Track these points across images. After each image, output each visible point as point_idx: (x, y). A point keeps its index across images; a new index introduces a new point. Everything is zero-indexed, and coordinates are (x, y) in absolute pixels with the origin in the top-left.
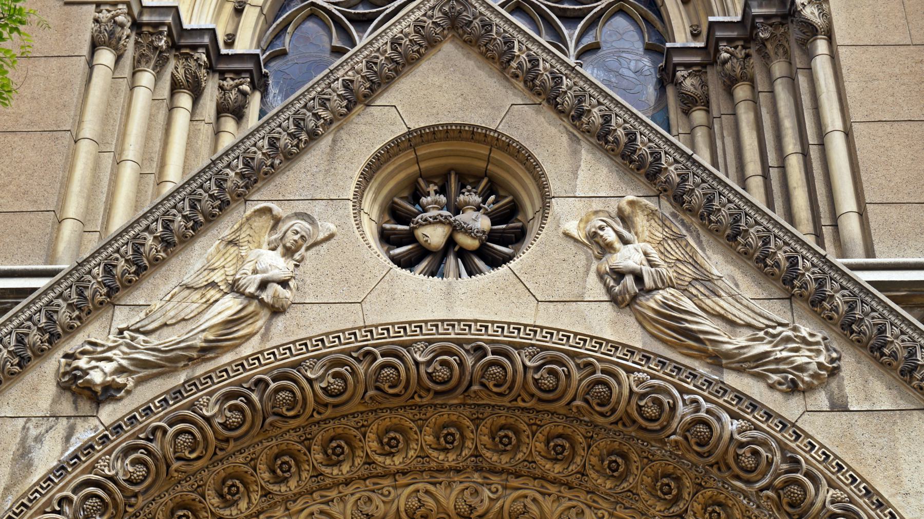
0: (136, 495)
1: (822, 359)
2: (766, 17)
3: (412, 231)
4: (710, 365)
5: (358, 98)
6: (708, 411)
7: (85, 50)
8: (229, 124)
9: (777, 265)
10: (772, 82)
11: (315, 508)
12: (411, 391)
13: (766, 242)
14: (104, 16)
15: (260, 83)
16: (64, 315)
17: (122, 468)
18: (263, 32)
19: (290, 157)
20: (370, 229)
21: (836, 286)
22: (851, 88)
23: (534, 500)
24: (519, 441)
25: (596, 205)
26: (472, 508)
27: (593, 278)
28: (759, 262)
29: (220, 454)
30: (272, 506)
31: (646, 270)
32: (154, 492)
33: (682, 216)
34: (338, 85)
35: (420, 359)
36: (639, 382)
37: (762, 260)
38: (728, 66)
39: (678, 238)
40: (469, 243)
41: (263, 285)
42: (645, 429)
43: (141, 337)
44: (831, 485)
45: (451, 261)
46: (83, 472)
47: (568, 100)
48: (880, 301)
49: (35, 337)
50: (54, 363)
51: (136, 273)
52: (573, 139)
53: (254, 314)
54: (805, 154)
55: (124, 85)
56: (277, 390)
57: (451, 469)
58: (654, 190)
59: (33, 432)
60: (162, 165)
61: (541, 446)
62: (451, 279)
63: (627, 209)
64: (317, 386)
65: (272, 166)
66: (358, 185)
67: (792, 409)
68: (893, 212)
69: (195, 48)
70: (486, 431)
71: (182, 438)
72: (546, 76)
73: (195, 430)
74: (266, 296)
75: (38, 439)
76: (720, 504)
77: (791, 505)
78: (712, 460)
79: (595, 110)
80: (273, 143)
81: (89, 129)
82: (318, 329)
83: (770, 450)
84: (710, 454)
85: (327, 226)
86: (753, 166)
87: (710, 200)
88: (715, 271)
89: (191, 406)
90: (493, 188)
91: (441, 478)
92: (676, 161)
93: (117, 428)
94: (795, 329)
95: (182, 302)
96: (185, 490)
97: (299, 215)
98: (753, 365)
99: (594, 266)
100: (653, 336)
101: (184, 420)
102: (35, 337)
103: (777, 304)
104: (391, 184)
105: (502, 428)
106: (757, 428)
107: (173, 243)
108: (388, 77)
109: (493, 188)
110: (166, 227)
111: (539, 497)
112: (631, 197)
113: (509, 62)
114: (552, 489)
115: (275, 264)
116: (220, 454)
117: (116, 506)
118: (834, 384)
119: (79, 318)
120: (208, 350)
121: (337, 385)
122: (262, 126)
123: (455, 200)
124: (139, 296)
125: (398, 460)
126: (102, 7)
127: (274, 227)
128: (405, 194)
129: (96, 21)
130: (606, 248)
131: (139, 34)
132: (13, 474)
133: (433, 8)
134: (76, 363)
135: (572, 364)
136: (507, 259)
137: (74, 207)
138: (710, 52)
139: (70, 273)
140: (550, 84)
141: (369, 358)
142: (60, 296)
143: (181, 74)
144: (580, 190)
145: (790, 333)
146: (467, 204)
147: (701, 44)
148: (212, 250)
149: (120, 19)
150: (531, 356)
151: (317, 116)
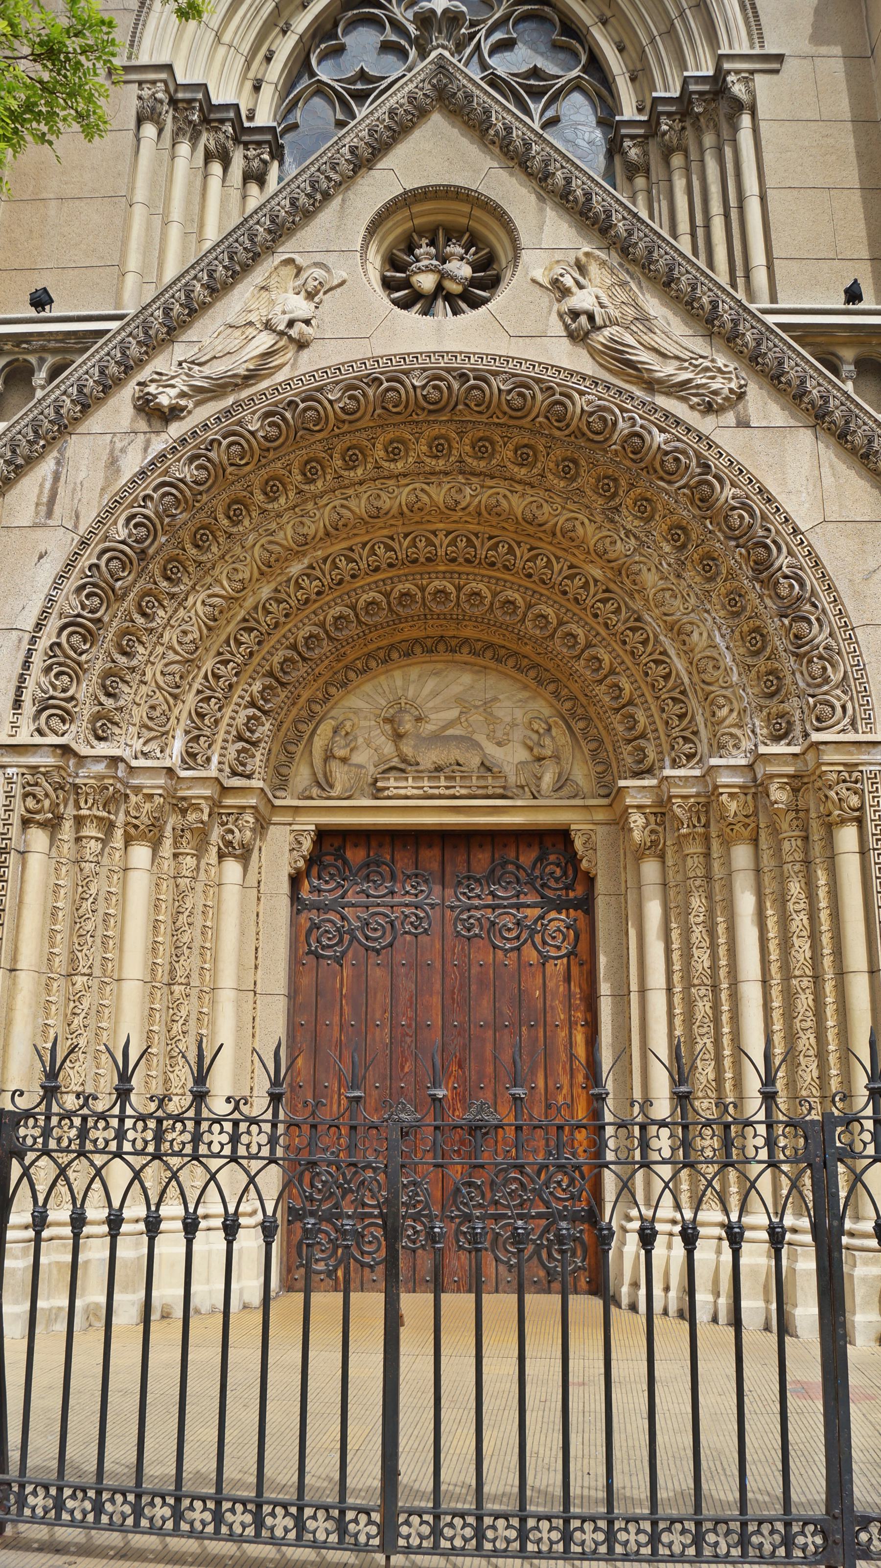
0: (201, 493)
1: (733, 385)
2: (701, 93)
3: (408, 277)
4: (645, 389)
5: (363, 161)
6: (642, 427)
7: (132, 124)
8: (253, 188)
9: (702, 307)
10: (702, 152)
11: (337, 503)
12: (410, 410)
13: (694, 289)
14: (146, 93)
15: (278, 153)
16: (134, 350)
17: (188, 472)
18: (278, 107)
19: (308, 215)
20: (375, 277)
21: (748, 325)
22: (767, 157)
23: (505, 496)
24: (493, 449)
25: (559, 255)
26: (457, 503)
27: (554, 317)
28: (688, 306)
29: (263, 461)
30: (305, 501)
31: (597, 311)
32: (214, 491)
33: (627, 266)
34: (345, 150)
35: (417, 384)
36: (589, 403)
37: (690, 304)
38: (667, 137)
39: (623, 284)
40: (455, 288)
41: (291, 324)
42: (592, 441)
43: (196, 368)
44: (733, 485)
45: (440, 302)
46: (159, 476)
47: (537, 163)
48: (782, 339)
49: (113, 369)
50: (128, 392)
51: (189, 315)
52: (541, 199)
53: (285, 348)
54: (727, 216)
55: (166, 155)
56: (305, 410)
57: (440, 472)
58: (605, 244)
59: (119, 445)
60: (202, 226)
61: (510, 454)
62: (440, 317)
63: (584, 260)
64: (336, 406)
65: (293, 222)
66: (364, 238)
67: (706, 424)
68: (794, 266)
69: (222, 121)
70: (468, 441)
71: (233, 448)
72: (519, 143)
73: (243, 442)
74: (294, 332)
75: (123, 450)
76: (647, 500)
77: (702, 500)
78: (643, 465)
79: (559, 173)
80: (293, 202)
81: (141, 194)
83: (688, 458)
84: (642, 460)
85: (340, 274)
86: (683, 226)
87: (650, 252)
88: (652, 312)
89: (239, 423)
90: (473, 241)
91: (433, 479)
92: (624, 218)
93: (183, 441)
94: (713, 361)
95: (227, 338)
96: (237, 490)
97: (317, 264)
98: (679, 390)
99: (556, 306)
100: (601, 365)
101: (234, 434)
102: (113, 369)
103: (700, 340)
104: (390, 238)
105: (480, 439)
106: (679, 440)
107: (217, 290)
108: (386, 144)
109: (473, 241)
110: (210, 276)
111: (508, 494)
112: (587, 249)
113: (487, 129)
114: (519, 488)
115: (301, 307)
116: (263, 461)
117: (186, 502)
119: (146, 353)
120: (250, 378)
121: (352, 405)
122: (280, 191)
123: (444, 249)
124: (192, 334)
125: (400, 465)
126: (144, 86)
127: (297, 275)
128: (402, 247)
129: (140, 98)
130: (565, 292)
131: (175, 110)
132: (106, 478)
133: (423, 81)
134: (147, 390)
135: (536, 388)
136: (485, 301)
137: (133, 262)
138: (652, 126)
139: (136, 316)
140: (522, 149)
141: (376, 383)
142: (130, 335)
143: (212, 146)
144: (546, 241)
145: (709, 364)
146: (452, 254)
147: (645, 118)
148: (248, 295)
149: (160, 95)
150: (505, 381)
151: (329, 179)
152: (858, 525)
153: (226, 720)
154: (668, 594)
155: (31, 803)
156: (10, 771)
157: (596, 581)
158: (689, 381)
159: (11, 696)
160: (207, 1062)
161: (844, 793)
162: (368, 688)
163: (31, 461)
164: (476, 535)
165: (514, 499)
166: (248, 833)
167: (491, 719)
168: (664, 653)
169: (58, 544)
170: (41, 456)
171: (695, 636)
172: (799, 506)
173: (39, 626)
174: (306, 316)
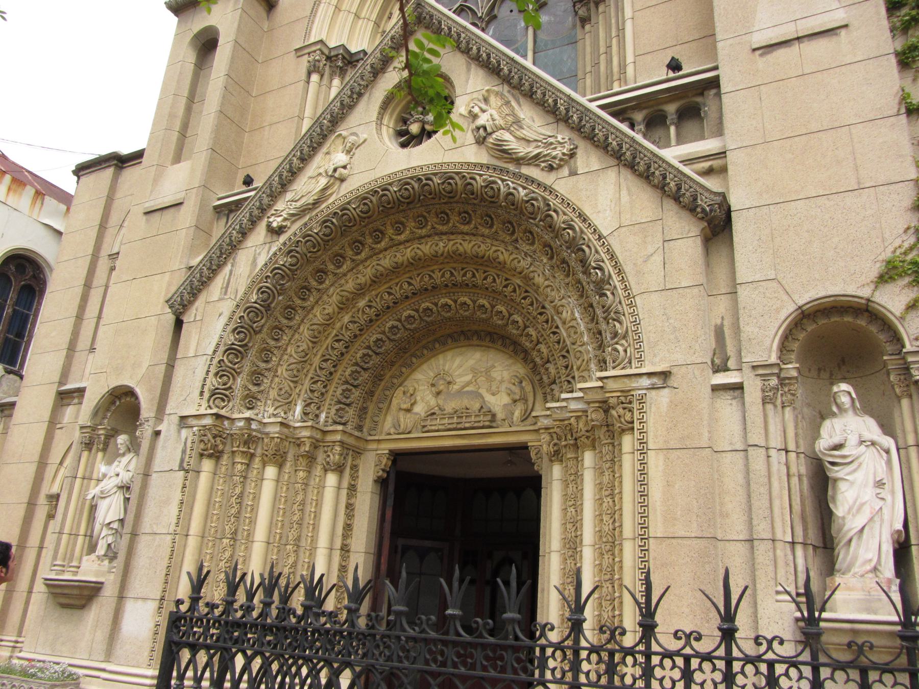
16: (266, 200)
19: (351, 107)
30: (358, 265)
36: (484, 180)
39: (508, 103)
41: (335, 170)
53: (333, 184)
74: (337, 175)
75: (259, 254)
82: (355, 186)
91: (423, 241)
95: (306, 187)
98: (534, 160)
107: (305, 159)
112: (487, 88)
114: (467, 237)
118: (572, 161)
120: (316, 203)
131: (331, 62)
152: (643, 226)
153: (331, 392)
154: (549, 289)
155: (202, 446)
156: (195, 429)
157: (519, 286)
158: (539, 154)
159: (199, 390)
160: (290, 589)
161: (621, 411)
162: (425, 367)
163: (220, 266)
164: (454, 269)
165: (465, 244)
166: (337, 457)
167: (490, 379)
168: (557, 327)
169: (227, 307)
170: (225, 263)
171: (564, 313)
172: (604, 221)
173: (215, 352)
174: (342, 164)
